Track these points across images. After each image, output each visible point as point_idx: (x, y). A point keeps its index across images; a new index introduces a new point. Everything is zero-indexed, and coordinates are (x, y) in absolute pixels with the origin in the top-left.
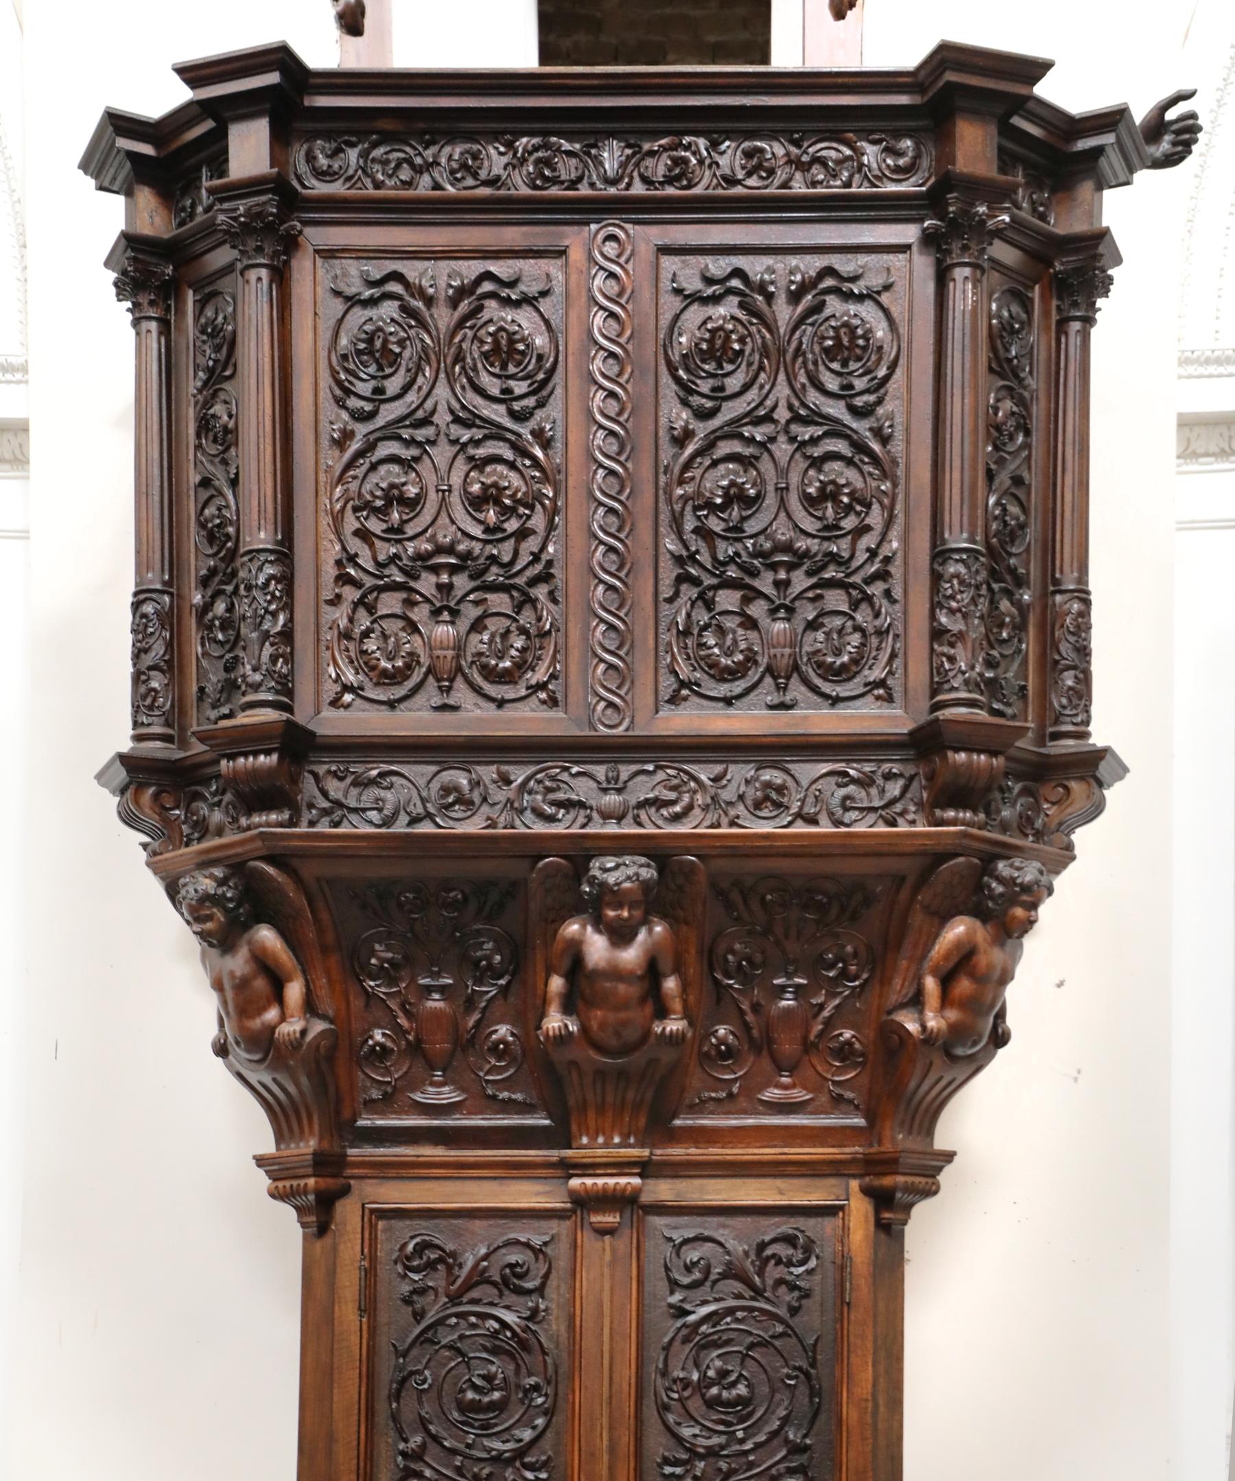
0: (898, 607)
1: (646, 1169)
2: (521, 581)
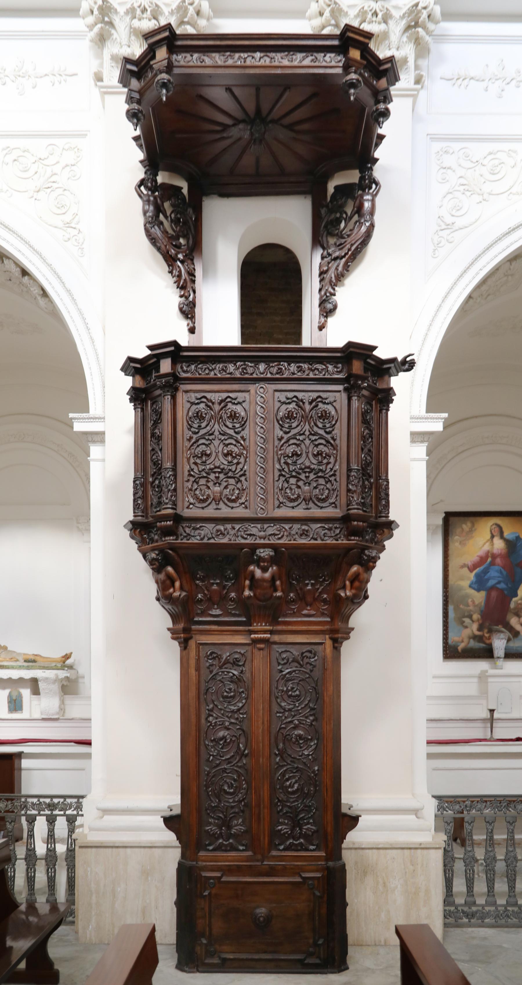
0: (338, 483)
1: (271, 632)
2: (237, 476)
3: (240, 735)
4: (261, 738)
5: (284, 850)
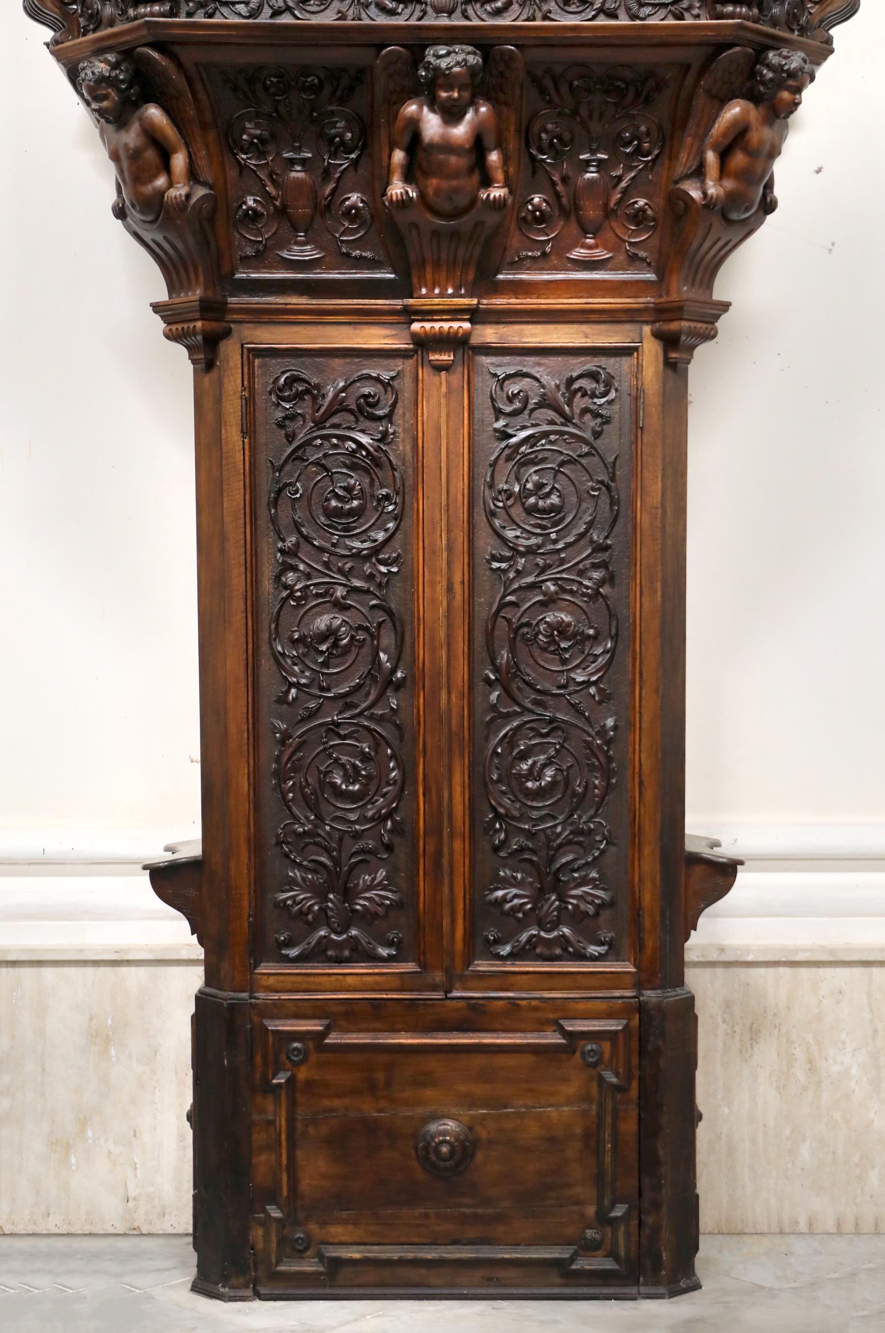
1: (475, 316)
3: (380, 624)
4: (442, 634)
5: (513, 956)
